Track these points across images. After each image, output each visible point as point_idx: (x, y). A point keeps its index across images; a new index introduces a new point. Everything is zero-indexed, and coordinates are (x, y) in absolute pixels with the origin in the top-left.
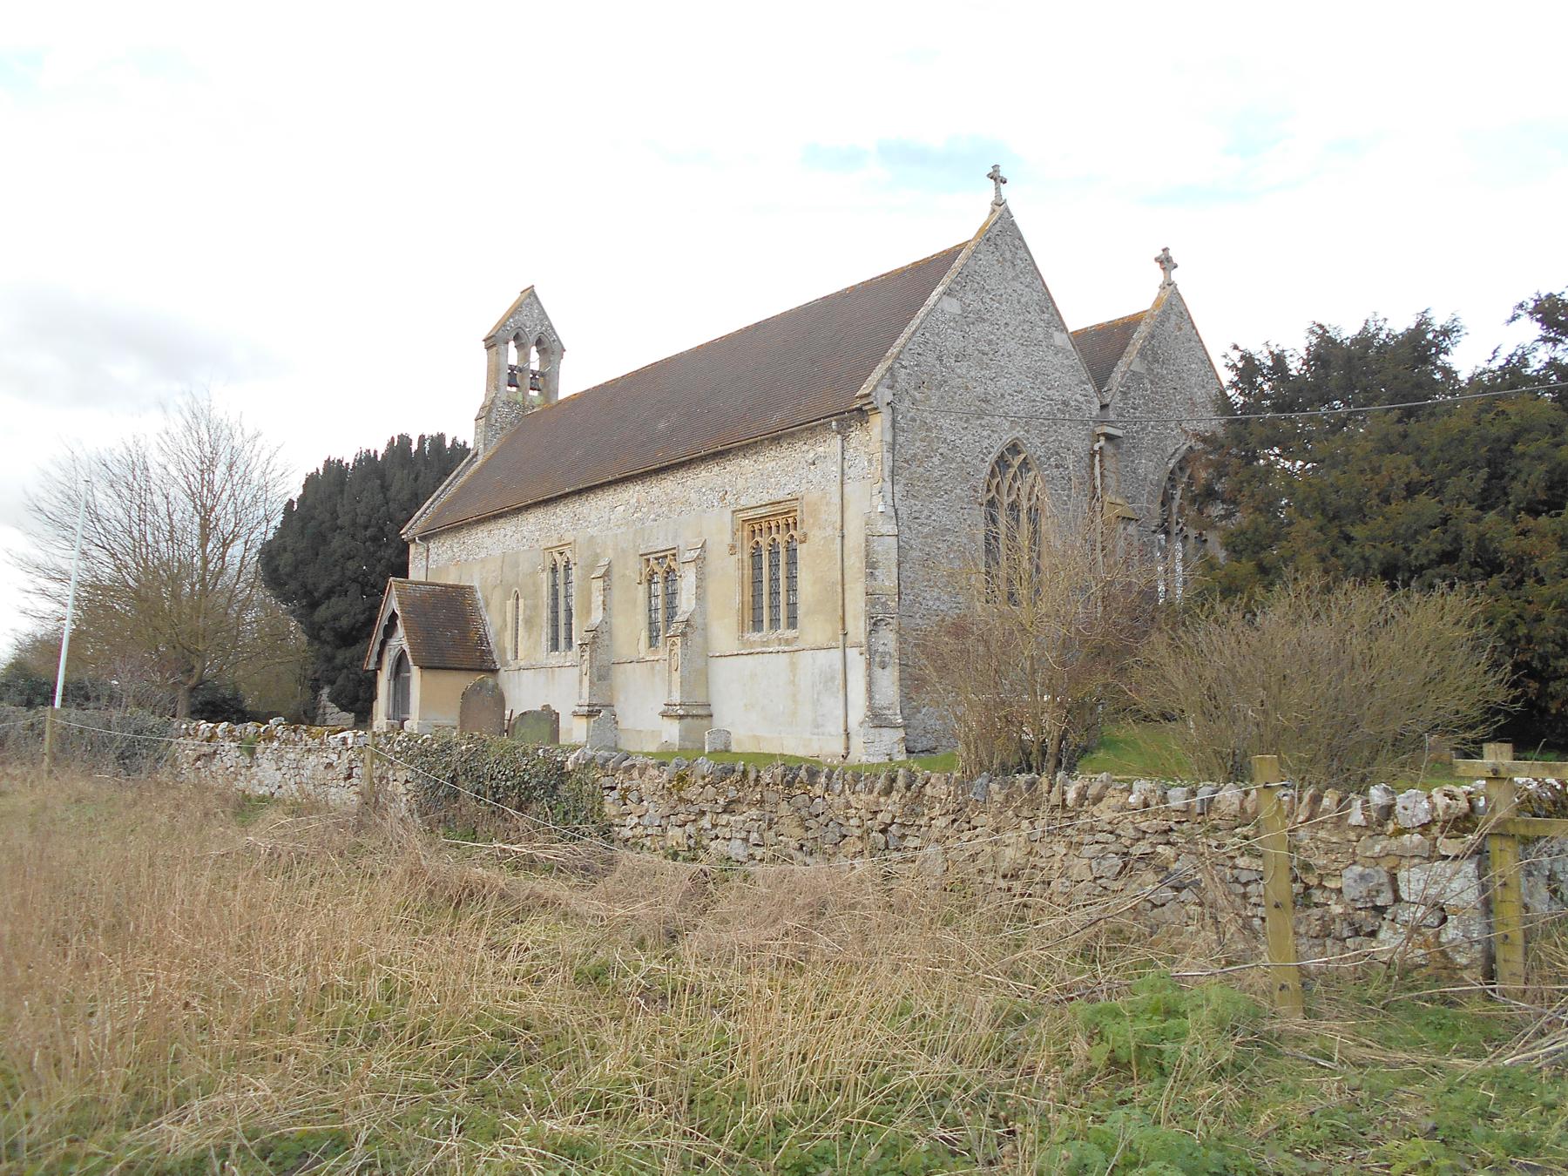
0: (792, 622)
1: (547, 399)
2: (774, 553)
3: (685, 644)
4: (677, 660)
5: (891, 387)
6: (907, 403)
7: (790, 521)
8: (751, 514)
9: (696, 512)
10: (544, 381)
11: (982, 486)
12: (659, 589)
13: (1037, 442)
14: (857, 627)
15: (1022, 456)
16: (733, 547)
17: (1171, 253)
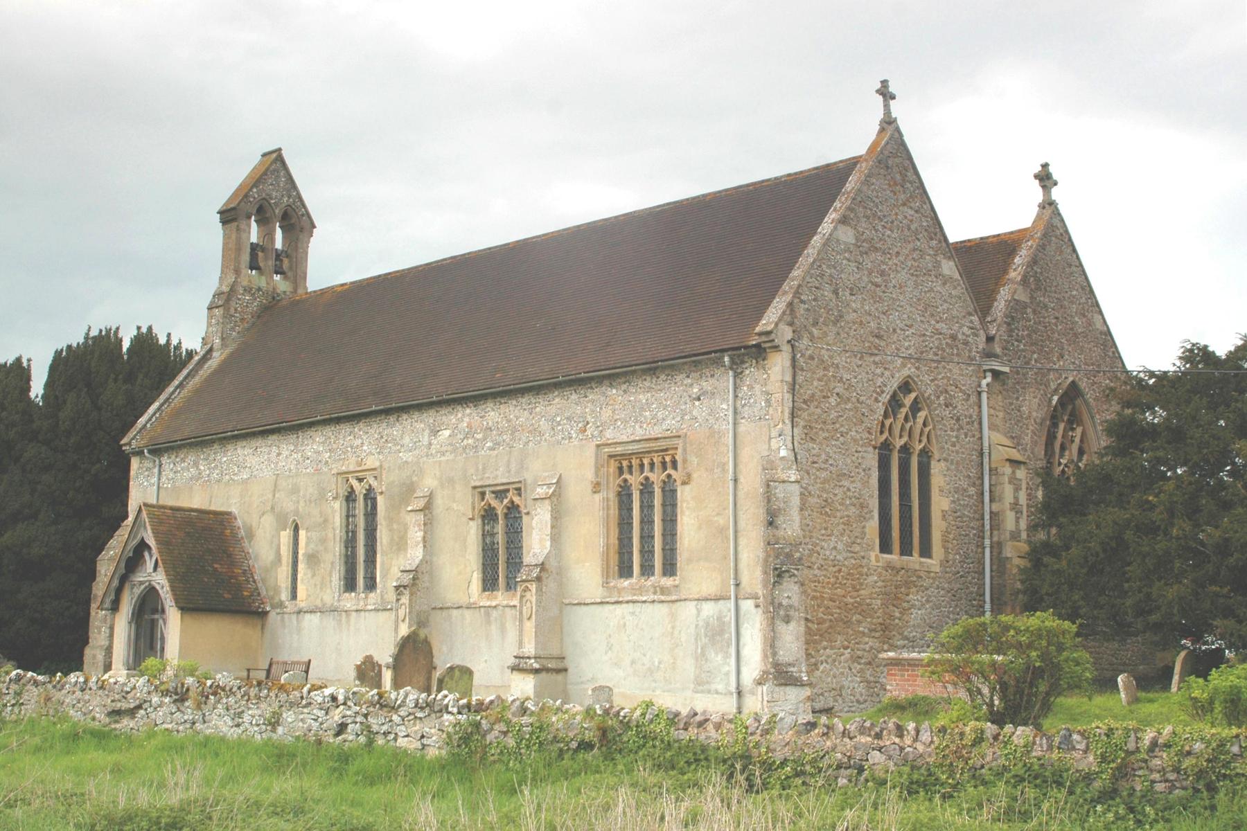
0: (670, 568)
1: (295, 290)
3: (539, 590)
5: (791, 324)
6: (805, 341)
7: (668, 459)
8: (619, 449)
9: (558, 447)
10: (290, 261)
11: (876, 427)
12: (500, 528)
13: (927, 379)
14: (753, 576)
15: (913, 395)
17: (1051, 169)
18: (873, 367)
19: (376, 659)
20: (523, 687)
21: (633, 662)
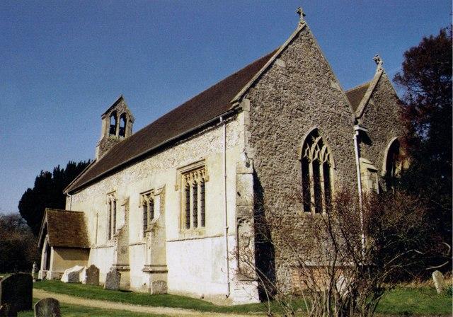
2: (195, 188)
4: (149, 244)
9: (162, 173)
15: (320, 138)
16: (176, 186)
18: (298, 123)
19: (96, 266)
20: (147, 278)
21: (190, 268)
